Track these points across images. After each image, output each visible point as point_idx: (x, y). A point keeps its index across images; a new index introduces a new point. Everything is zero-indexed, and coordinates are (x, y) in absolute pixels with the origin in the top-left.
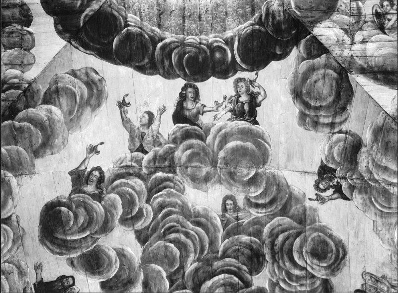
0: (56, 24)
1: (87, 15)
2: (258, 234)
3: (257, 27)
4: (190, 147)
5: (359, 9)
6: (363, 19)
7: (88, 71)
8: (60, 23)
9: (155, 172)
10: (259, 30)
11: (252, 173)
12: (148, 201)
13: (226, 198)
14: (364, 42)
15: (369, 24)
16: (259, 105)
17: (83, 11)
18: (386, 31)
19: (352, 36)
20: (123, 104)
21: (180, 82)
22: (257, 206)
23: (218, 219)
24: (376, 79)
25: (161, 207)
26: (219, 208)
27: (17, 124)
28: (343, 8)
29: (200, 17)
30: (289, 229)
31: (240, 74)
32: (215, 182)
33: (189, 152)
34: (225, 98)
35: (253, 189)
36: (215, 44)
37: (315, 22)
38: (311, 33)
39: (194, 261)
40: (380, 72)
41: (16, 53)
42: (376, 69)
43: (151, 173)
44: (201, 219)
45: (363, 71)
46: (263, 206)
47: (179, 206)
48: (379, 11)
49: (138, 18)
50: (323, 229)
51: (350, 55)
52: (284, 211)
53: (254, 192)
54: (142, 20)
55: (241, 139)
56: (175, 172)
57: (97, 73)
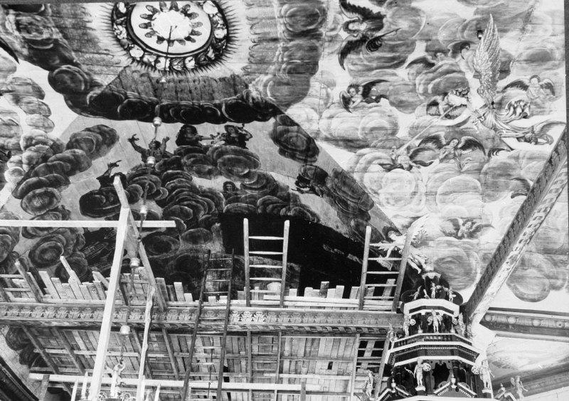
0: (66, 100)
1: (91, 97)
2: (254, 203)
3: (240, 101)
4: (194, 156)
5: (328, 95)
6: (330, 101)
7: (99, 127)
8: (69, 99)
9: (166, 170)
10: (241, 103)
11: (246, 171)
12: (163, 186)
13: (225, 184)
14: (331, 117)
15: (337, 104)
16: (248, 140)
17: (88, 93)
18: (350, 110)
19: (320, 114)
20: (132, 140)
21: (180, 125)
22: (251, 189)
23: (221, 194)
24: (337, 145)
25: (174, 188)
26: (222, 189)
27: (49, 164)
28: (314, 93)
29: (190, 92)
30: (276, 203)
31: (228, 123)
32: (217, 175)
33: (192, 159)
34: (219, 134)
35: (247, 180)
36: (206, 106)
37: (288, 105)
38: (282, 113)
39: (205, 214)
40: (341, 140)
41: (36, 118)
42: (338, 138)
43: (163, 171)
44: (211, 194)
45: (327, 139)
46: (255, 189)
47: (189, 187)
48: (345, 95)
49: (137, 94)
50: (303, 206)
51: (317, 129)
52: (273, 193)
53: (247, 182)
54: (139, 93)
55: (235, 155)
56: (183, 170)
57: (107, 127)
